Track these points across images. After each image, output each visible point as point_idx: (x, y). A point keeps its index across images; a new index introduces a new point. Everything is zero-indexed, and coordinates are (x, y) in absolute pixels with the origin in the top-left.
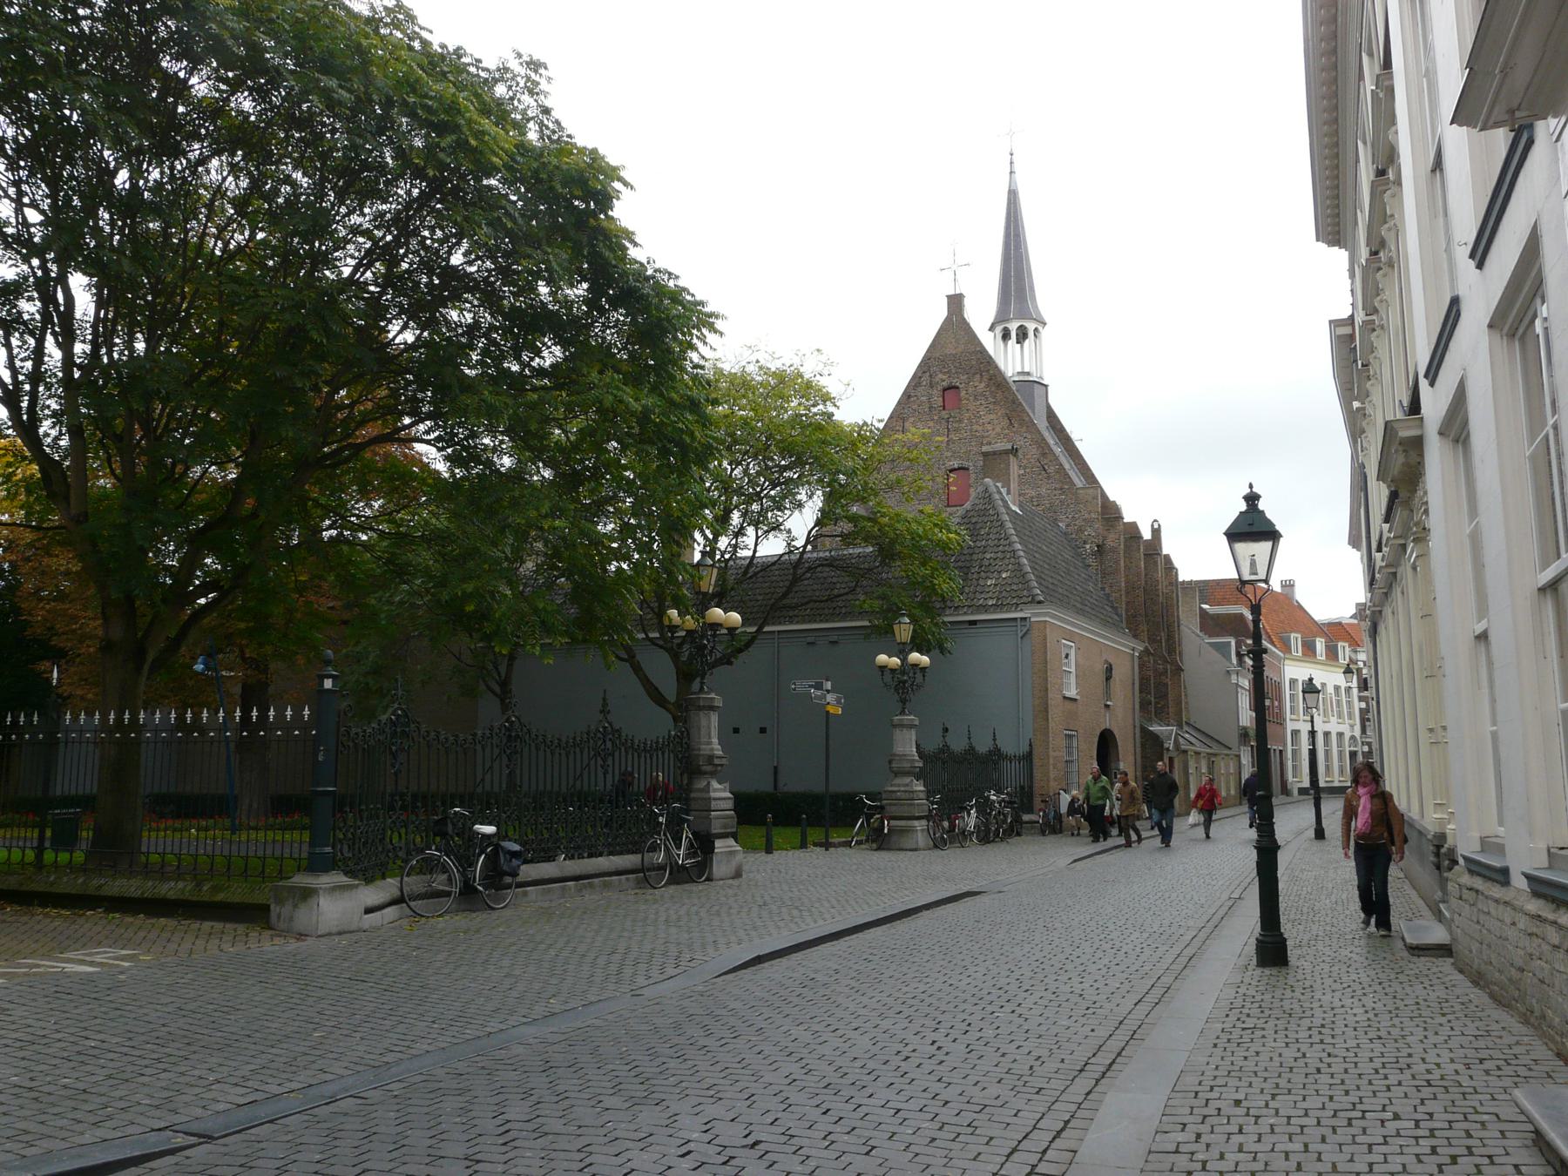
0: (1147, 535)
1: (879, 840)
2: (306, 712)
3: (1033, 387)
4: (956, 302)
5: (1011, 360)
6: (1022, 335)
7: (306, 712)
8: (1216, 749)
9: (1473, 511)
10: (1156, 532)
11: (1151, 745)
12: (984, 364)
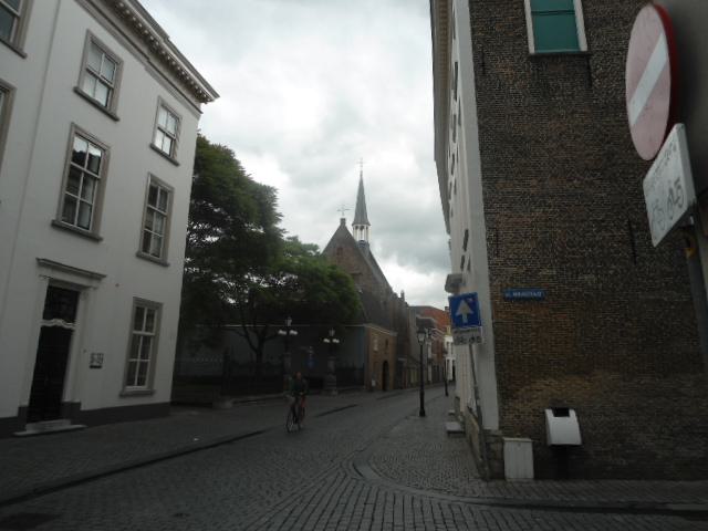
0: (399, 296)
1: (211, 100)
2: (232, 301)
3: (365, 245)
4: (343, 221)
5: (358, 236)
6: (362, 228)
7: (232, 301)
8: (360, 478)
9: (662, 145)
10: (403, 294)
11: (399, 365)
12: (350, 239)
